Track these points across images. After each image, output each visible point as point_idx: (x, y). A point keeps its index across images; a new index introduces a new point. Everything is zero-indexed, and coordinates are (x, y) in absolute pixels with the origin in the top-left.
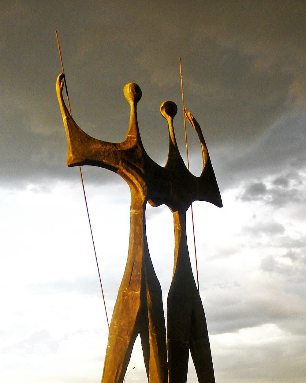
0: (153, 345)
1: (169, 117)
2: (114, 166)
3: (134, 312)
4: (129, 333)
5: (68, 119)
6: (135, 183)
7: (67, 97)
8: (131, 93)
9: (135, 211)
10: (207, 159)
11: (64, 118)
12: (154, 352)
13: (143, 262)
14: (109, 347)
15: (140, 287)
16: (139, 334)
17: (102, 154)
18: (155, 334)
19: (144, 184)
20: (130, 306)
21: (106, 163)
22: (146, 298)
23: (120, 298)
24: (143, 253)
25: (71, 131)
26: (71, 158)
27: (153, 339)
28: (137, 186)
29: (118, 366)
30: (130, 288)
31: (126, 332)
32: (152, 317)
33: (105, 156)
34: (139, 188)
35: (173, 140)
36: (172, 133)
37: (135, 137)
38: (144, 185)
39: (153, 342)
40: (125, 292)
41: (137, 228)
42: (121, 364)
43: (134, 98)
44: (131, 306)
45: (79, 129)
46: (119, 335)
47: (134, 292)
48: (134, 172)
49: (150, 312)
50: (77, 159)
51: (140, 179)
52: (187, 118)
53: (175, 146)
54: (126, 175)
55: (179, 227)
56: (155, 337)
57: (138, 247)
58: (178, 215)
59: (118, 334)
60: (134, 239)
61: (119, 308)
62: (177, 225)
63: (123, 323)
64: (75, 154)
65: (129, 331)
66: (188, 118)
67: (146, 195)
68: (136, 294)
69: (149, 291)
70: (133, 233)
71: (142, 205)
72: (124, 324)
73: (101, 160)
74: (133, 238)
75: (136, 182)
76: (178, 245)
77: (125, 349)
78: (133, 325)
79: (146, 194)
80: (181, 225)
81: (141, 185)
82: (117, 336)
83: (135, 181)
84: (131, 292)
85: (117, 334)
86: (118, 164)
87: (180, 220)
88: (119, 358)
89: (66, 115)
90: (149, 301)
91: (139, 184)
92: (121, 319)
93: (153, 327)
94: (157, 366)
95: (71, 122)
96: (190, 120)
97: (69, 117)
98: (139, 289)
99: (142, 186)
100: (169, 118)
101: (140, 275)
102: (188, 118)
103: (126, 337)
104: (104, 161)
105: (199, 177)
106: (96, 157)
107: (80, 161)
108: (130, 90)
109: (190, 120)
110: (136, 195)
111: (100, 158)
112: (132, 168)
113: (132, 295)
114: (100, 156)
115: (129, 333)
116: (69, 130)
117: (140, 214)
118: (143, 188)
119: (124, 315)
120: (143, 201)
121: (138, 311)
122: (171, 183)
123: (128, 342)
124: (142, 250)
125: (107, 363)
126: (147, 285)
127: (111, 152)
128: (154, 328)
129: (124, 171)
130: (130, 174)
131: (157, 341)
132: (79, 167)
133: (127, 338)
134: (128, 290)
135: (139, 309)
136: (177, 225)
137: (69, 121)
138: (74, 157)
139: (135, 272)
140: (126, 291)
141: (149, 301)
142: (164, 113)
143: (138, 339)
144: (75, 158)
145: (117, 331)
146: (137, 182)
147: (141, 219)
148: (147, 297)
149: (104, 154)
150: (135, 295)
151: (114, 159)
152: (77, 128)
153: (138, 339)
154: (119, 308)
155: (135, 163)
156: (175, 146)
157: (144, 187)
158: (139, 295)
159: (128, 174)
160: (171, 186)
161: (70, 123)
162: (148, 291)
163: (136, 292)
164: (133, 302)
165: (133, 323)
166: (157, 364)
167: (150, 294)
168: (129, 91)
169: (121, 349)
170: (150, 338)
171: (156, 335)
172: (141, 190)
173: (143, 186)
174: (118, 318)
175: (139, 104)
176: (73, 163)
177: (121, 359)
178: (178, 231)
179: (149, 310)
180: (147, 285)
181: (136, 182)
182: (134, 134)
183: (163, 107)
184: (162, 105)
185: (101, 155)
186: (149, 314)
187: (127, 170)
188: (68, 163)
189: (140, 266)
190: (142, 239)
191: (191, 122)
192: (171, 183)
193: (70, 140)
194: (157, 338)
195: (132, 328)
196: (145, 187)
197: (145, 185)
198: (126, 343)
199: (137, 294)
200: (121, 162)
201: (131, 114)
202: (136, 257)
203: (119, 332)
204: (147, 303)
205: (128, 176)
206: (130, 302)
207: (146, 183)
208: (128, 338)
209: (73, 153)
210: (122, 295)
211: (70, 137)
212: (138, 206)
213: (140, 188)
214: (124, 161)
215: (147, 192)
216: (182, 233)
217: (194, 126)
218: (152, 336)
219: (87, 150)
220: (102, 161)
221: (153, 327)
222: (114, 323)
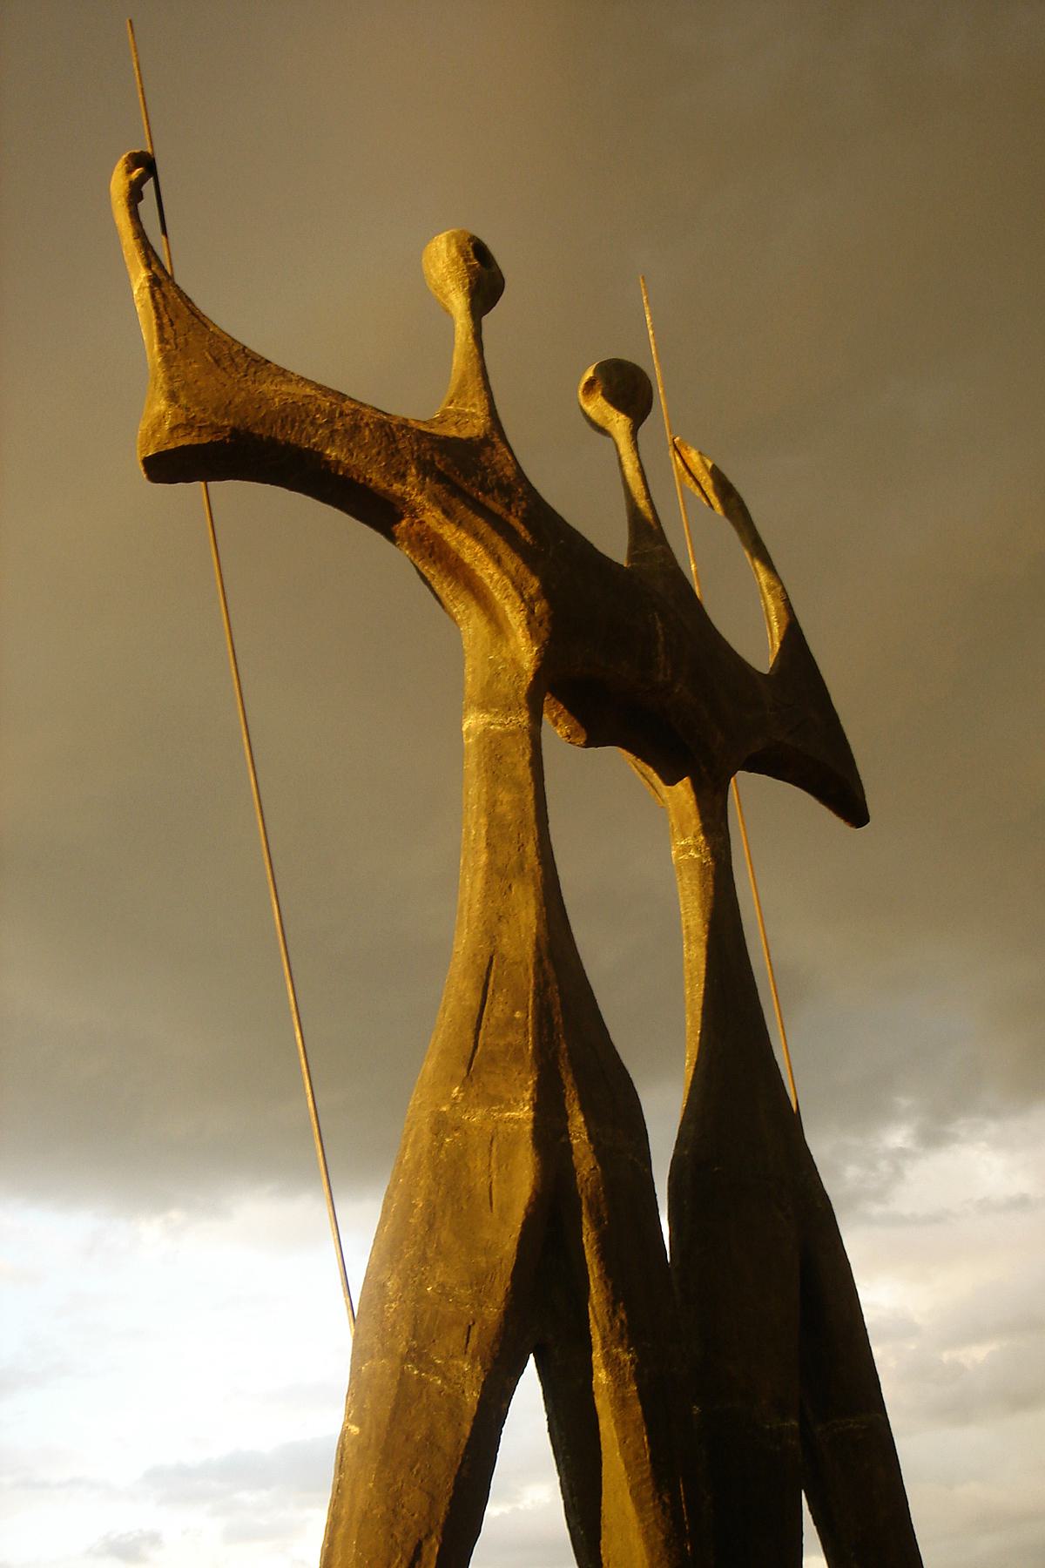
0: (621, 1423)
1: (622, 417)
2: (384, 485)
3: (503, 1220)
4: (473, 1341)
5: (154, 282)
6: (487, 581)
7: (163, 237)
8: (454, 262)
9: (488, 718)
10: (785, 621)
11: (139, 278)
12: (628, 1466)
13: (539, 962)
14: (355, 1429)
15: (530, 1083)
16: (532, 1358)
17: (320, 422)
18: (628, 1357)
19: (534, 584)
20: (479, 1185)
21: (338, 462)
22: (568, 1148)
23: (415, 1142)
24: (538, 917)
25: (165, 320)
26: (161, 418)
27: (618, 1381)
28: (497, 595)
29: (410, 1547)
30: (473, 1091)
31: (458, 1332)
32: (604, 1255)
33: (333, 432)
34: (507, 608)
35: (642, 504)
36: (638, 477)
37: (480, 413)
38: (532, 591)
39: (621, 1403)
40: (444, 1109)
41: (505, 797)
42: (427, 1537)
43: (470, 282)
44: (481, 1182)
45: (209, 324)
46: (417, 1355)
47: (500, 1111)
48: (483, 527)
49: (597, 1223)
50: (189, 425)
51: (513, 562)
52: (686, 474)
53: (652, 522)
54: (438, 537)
55: (697, 849)
56: (629, 1370)
57: (510, 887)
58: (693, 796)
59: (411, 1349)
60: (488, 844)
61: (411, 1197)
62: (690, 841)
63: (442, 1285)
64: (183, 401)
65: (475, 1331)
66: (691, 474)
67: (544, 645)
68: (511, 1120)
69: (583, 1109)
70: (483, 820)
71: (522, 694)
72: (444, 1292)
73: (315, 444)
74: (483, 844)
75: (491, 576)
76: (700, 933)
77: (455, 1437)
78: (500, 1296)
79: (544, 635)
80: (708, 841)
81: (519, 588)
82: (405, 1359)
83: (487, 572)
84: (481, 1112)
85: (402, 1348)
86: (402, 477)
87: (702, 818)
88: (414, 1500)
89: (148, 266)
90: (585, 1162)
91: (507, 581)
92: (423, 1259)
93: (615, 1313)
94: (651, 1550)
95: (172, 294)
96: (698, 484)
97: (162, 277)
98: (527, 1095)
99: (521, 595)
100: (619, 424)
101: (530, 1024)
102: (691, 474)
103: (458, 1369)
104: (332, 453)
105: (739, 772)
106: (288, 427)
107: (205, 440)
108: (454, 250)
109: (698, 484)
110: (494, 645)
111: (309, 438)
112: (470, 508)
113: (489, 1128)
114: (310, 429)
115: (473, 1341)
116: (159, 317)
117: (513, 734)
118: (529, 604)
119: (445, 1235)
120: (530, 674)
121: (526, 1213)
122: (659, 625)
123: (472, 1397)
124: (533, 902)
125: (341, 1531)
126: (568, 1080)
127: (367, 425)
128: (623, 1316)
129: (433, 518)
130: (464, 535)
131: (643, 1395)
132: (202, 483)
133: (464, 1374)
134: (464, 1099)
135: (531, 1204)
136: (690, 841)
137: (163, 289)
138: (175, 416)
139: (498, 1009)
140: (454, 1105)
141: (585, 1162)
142: (597, 407)
143: (529, 1392)
144: (182, 420)
145: (405, 1328)
146: (496, 577)
147: (523, 755)
148: (575, 1142)
149: (331, 421)
150: (501, 1127)
151: (379, 453)
152: (197, 317)
153: (529, 1392)
154: (411, 1197)
155: (486, 493)
156: (652, 522)
157: (532, 600)
158: (529, 1127)
159: (451, 535)
160: (660, 632)
161: (164, 296)
162: (576, 1107)
163: (509, 1111)
164: (493, 1165)
165: (501, 1285)
166: (646, 1535)
167: (586, 1122)
168: (448, 251)
169: (431, 1439)
170: (601, 1376)
171: (632, 1361)
172: (515, 617)
173: (526, 597)
174: (410, 1253)
175: (486, 320)
176: (171, 446)
177: (433, 1500)
178: (698, 867)
179: (590, 1209)
180: (568, 1080)
181: (491, 576)
182: (474, 405)
183: (590, 385)
184: (589, 374)
185: (313, 423)
186: (588, 1237)
187: (449, 514)
188: (146, 447)
189: (527, 981)
190: (531, 848)
191: (703, 492)
192: (659, 625)
193: (161, 350)
194: (638, 1376)
195: (493, 1311)
196: (538, 599)
197: (538, 590)
198: (455, 1402)
199: (517, 1121)
200: (414, 471)
201: (457, 341)
202: (500, 935)
203: (414, 1337)
204: (572, 1172)
205: (453, 544)
206: (478, 1164)
207: (541, 581)
208: (472, 1369)
209: (172, 397)
210: (426, 1128)
211: (162, 340)
212: (506, 697)
213: (513, 604)
214: (426, 468)
215: (546, 625)
216: (716, 879)
217: (717, 506)
218: (611, 1363)
219: (243, 394)
220: (321, 454)
221: (615, 1313)
222: (384, 1286)
